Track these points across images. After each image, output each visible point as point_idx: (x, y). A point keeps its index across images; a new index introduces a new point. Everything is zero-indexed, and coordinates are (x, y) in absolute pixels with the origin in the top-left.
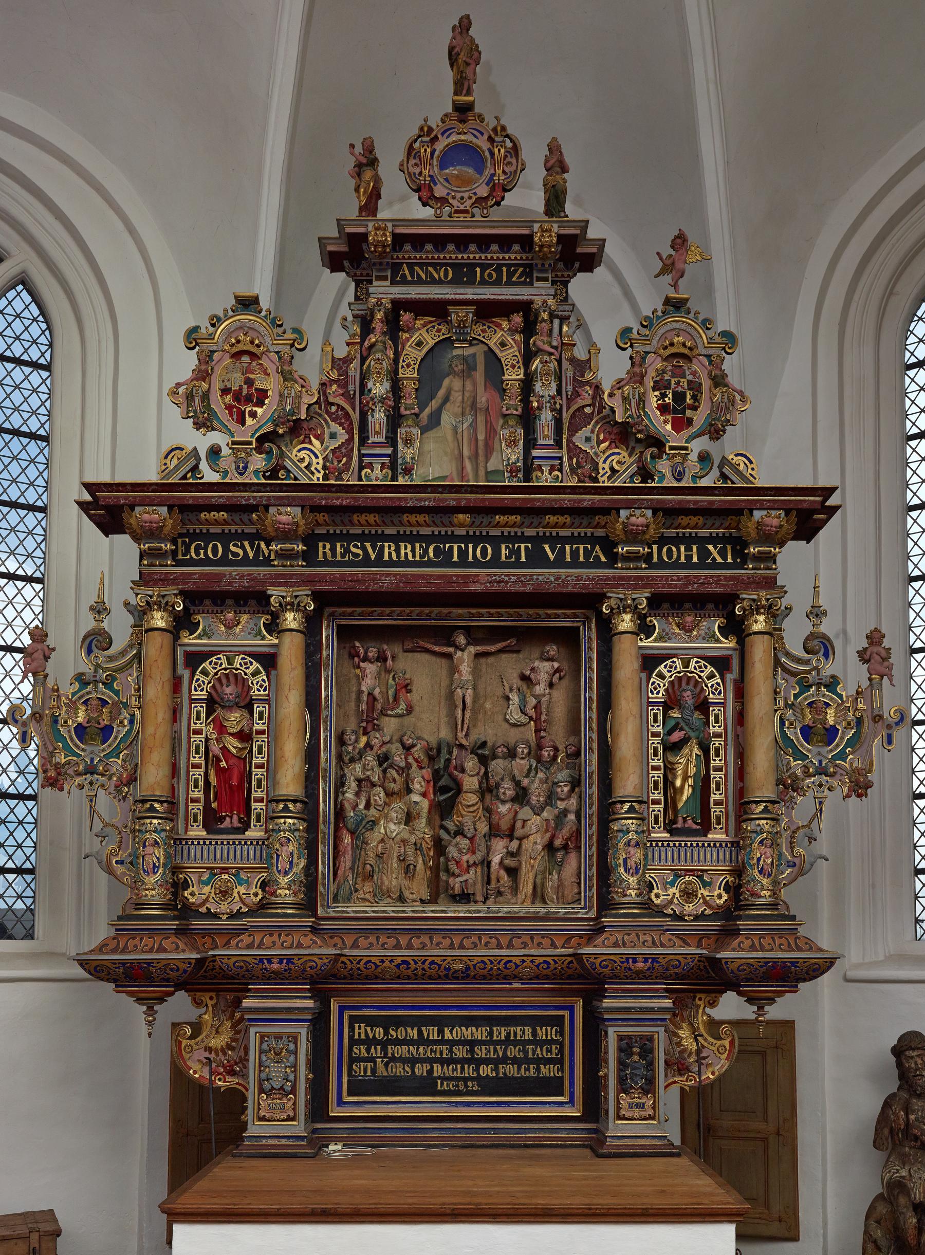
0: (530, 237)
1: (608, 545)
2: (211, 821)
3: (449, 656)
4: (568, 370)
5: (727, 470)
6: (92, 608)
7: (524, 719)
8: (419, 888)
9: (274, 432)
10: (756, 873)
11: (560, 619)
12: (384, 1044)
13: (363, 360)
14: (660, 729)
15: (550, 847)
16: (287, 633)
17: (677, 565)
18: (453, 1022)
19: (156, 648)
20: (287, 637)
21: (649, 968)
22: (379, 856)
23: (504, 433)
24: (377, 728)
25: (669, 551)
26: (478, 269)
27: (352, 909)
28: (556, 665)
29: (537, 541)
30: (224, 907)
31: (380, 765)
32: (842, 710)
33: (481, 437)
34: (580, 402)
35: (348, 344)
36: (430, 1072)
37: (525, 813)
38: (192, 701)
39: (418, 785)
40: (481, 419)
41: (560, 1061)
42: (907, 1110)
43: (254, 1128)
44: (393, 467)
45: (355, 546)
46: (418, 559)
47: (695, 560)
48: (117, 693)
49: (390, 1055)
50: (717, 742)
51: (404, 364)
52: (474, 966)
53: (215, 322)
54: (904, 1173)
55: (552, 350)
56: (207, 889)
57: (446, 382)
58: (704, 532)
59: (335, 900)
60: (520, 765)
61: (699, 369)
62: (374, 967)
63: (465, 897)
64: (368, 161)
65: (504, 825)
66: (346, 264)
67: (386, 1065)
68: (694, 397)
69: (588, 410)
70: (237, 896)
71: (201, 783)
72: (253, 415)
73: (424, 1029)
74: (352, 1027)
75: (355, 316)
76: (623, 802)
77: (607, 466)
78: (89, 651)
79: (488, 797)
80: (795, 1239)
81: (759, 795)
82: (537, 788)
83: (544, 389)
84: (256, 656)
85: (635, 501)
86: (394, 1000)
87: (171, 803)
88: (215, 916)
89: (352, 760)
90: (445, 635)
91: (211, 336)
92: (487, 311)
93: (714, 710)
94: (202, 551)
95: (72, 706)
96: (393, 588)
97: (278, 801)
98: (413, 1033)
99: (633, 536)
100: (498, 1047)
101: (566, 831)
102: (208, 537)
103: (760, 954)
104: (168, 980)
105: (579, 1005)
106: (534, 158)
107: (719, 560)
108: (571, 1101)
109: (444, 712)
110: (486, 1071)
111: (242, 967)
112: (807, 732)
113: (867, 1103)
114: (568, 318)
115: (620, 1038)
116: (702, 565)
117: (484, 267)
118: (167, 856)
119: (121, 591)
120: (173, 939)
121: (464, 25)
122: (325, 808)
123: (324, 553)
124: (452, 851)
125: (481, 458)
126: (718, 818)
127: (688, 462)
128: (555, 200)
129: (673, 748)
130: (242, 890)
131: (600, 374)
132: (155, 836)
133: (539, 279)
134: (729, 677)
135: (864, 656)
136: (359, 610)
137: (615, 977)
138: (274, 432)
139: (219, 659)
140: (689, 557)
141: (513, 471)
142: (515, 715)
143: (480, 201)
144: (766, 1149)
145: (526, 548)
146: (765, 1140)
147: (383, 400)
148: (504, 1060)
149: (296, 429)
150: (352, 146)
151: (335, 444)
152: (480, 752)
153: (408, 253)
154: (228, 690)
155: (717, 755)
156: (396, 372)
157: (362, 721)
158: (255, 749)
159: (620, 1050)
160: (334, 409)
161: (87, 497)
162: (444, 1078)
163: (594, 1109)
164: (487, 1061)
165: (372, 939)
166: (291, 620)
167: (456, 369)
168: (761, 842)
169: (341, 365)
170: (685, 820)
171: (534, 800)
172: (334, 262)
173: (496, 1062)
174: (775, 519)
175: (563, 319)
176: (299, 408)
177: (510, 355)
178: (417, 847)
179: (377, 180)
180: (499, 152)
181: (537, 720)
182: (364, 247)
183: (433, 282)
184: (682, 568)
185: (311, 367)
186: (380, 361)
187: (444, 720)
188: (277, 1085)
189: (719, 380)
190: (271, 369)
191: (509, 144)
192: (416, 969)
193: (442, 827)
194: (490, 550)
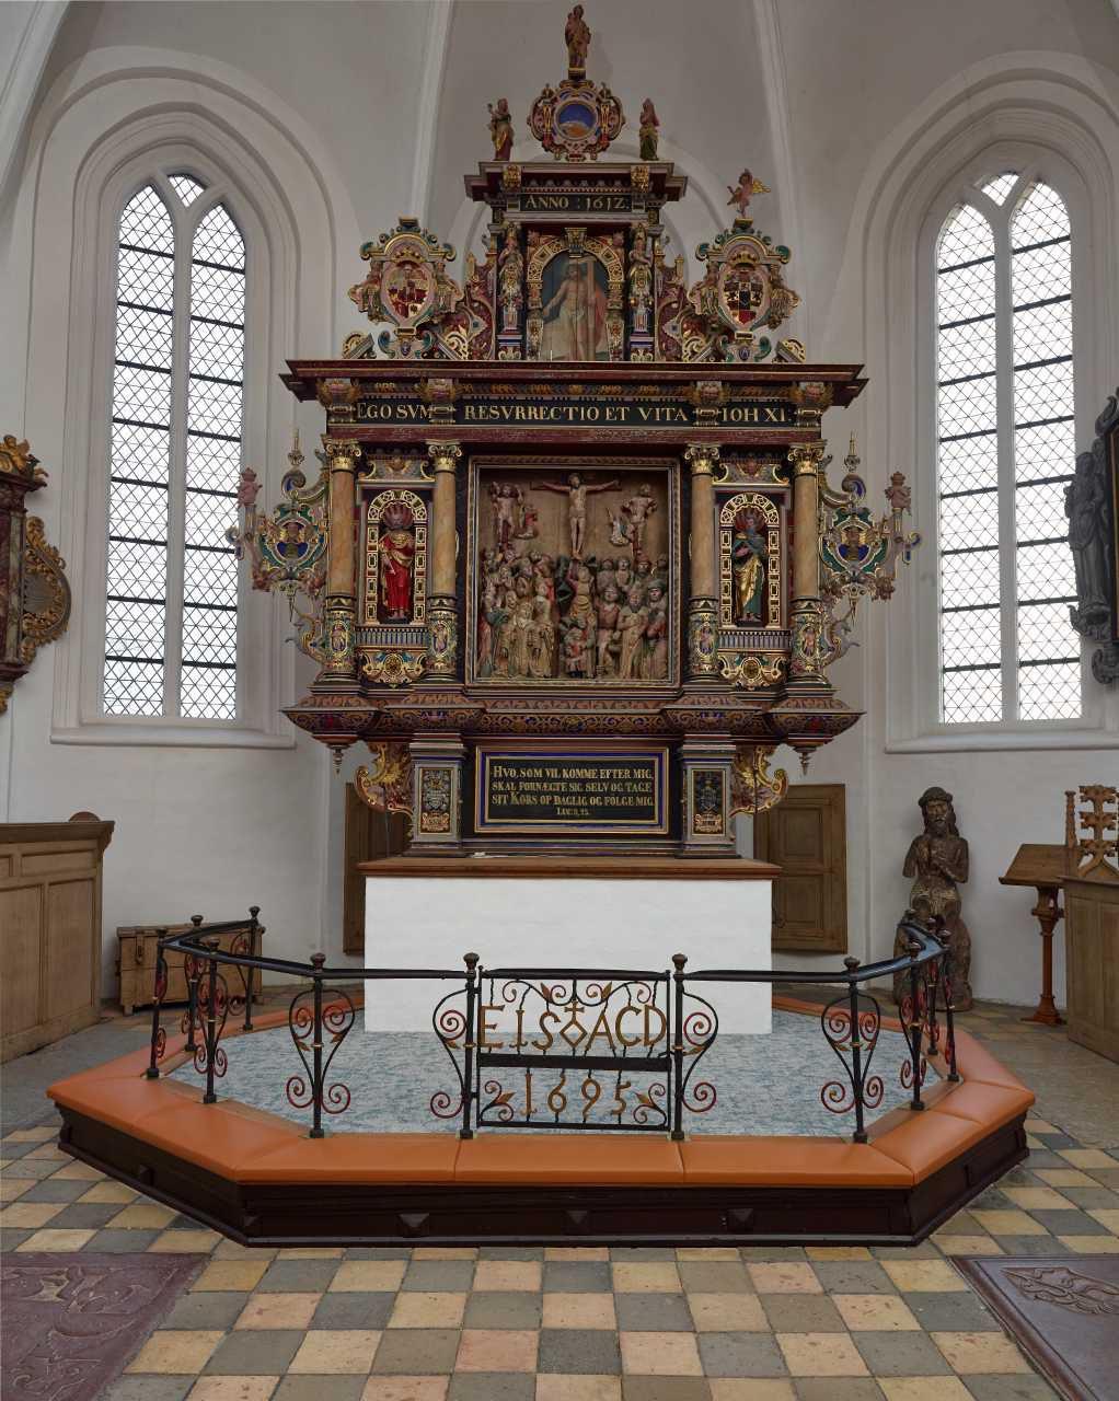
0: (629, 175)
1: (688, 408)
2: (383, 614)
3: (566, 493)
4: (659, 277)
5: (782, 352)
6: (290, 456)
7: (625, 541)
9: (431, 323)
10: (801, 652)
11: (653, 464)
12: (517, 781)
13: (499, 268)
15: (644, 637)
17: (742, 423)
18: (570, 765)
19: (339, 485)
20: (441, 477)
22: (513, 643)
23: (609, 323)
24: (510, 547)
25: (736, 413)
27: (492, 681)
28: (650, 500)
29: (634, 405)
30: (393, 679)
32: (871, 533)
33: (591, 326)
34: (668, 300)
35: (487, 256)
36: (552, 801)
37: (625, 610)
38: (368, 525)
39: (542, 589)
40: (591, 312)
41: (653, 795)
42: (930, 847)
43: (419, 837)
44: (523, 350)
47: (756, 419)
48: (310, 519)
50: (773, 557)
54: (926, 893)
56: (380, 665)
57: (564, 285)
58: (763, 399)
59: (479, 675)
60: (621, 575)
61: (761, 275)
63: (579, 674)
64: (502, 118)
65: (609, 619)
66: (486, 194)
67: (518, 796)
68: (757, 296)
69: (675, 306)
71: (376, 586)
72: (414, 309)
74: (492, 769)
75: (493, 235)
76: (699, 600)
77: (688, 349)
78: (288, 488)
79: (597, 599)
81: (803, 595)
82: (635, 593)
83: (640, 290)
84: (418, 492)
85: (709, 375)
86: (525, 748)
88: (387, 686)
89: (491, 571)
90: (563, 477)
91: (381, 250)
92: (595, 231)
93: (771, 534)
95: (275, 529)
96: (523, 440)
97: (434, 598)
98: (539, 773)
99: (708, 401)
101: (657, 625)
102: (380, 402)
103: (801, 710)
104: (352, 728)
105: (666, 753)
106: (632, 114)
108: (660, 823)
109: (562, 535)
110: (595, 801)
112: (844, 550)
113: (899, 846)
114: (658, 236)
115: (697, 774)
116: (761, 423)
117: (593, 198)
118: (352, 639)
119: (313, 442)
120: (356, 698)
121: (578, 12)
122: (471, 605)
124: (569, 639)
125: (591, 344)
126: (774, 614)
127: (757, 341)
128: (648, 148)
129: (739, 561)
130: (407, 665)
132: (341, 623)
133: (636, 207)
134: (783, 508)
135: (890, 494)
136: (496, 457)
137: (692, 728)
138: (431, 323)
140: (751, 418)
141: (616, 353)
142: (617, 537)
143: (590, 148)
148: (609, 793)
149: (449, 320)
150: (490, 106)
153: (534, 186)
154: (396, 517)
155: (774, 567)
156: (525, 277)
158: (417, 561)
159: (696, 782)
160: (476, 305)
161: (288, 372)
162: (562, 807)
163: (677, 828)
164: (595, 794)
165: (507, 703)
166: (444, 464)
168: (806, 630)
169: (481, 271)
170: (748, 616)
171: (632, 601)
172: (477, 193)
173: (602, 795)
174: (816, 388)
175: (655, 237)
177: (614, 263)
178: (542, 636)
179: (510, 132)
180: (605, 110)
181: (634, 542)
183: (554, 209)
184: (747, 426)
185: (457, 272)
186: (513, 269)
187: (562, 541)
188: (436, 806)
189: (776, 284)
190: (428, 275)
191: (613, 104)
193: (561, 621)
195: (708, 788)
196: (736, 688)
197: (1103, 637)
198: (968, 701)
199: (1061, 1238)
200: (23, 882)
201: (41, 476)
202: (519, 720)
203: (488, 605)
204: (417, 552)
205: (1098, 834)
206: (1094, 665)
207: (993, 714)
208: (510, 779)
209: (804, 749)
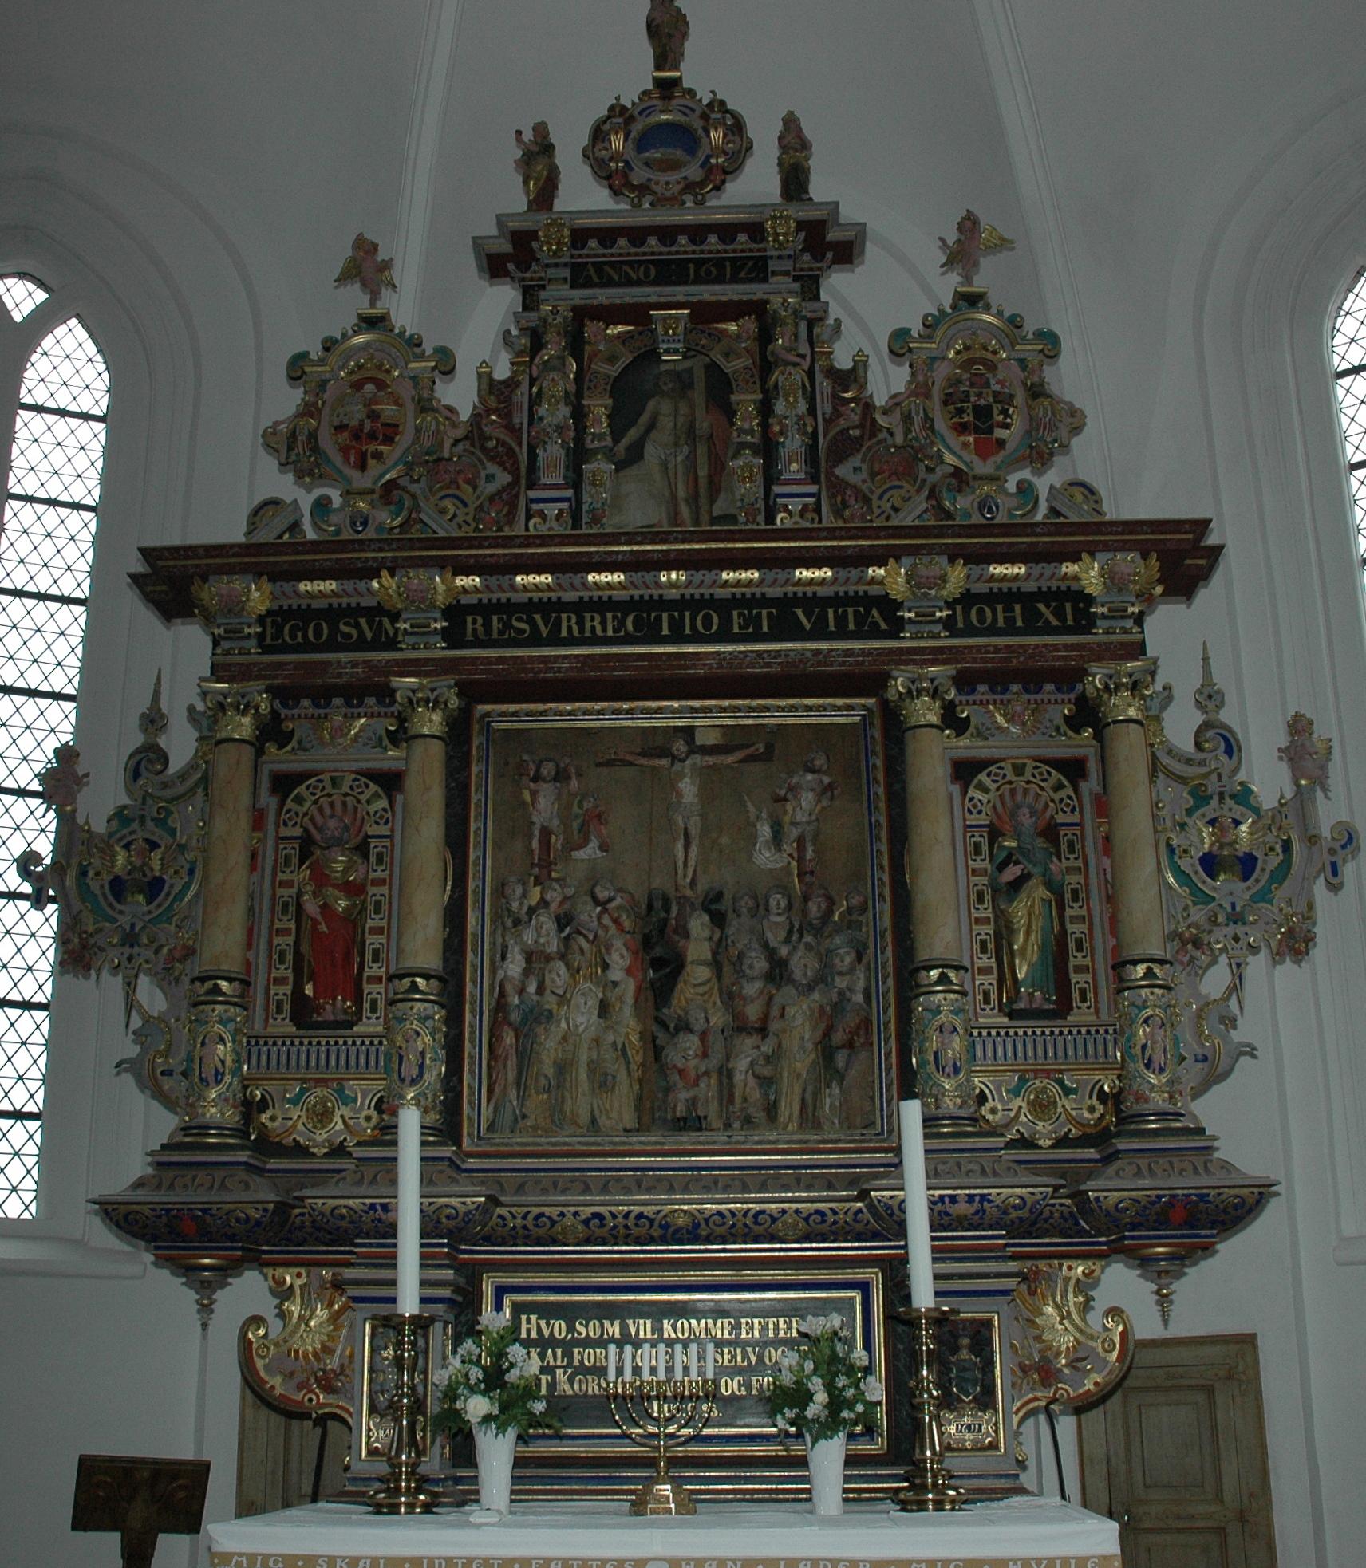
4: (824, 385)
8: (620, 1108)
12: (567, 1347)
14: (987, 865)
15: (827, 1052)
16: (420, 741)
21: (977, 1212)
25: (981, 612)
26: (691, 266)
28: (826, 780)
31: (561, 929)
33: (703, 472)
40: (701, 450)
45: (519, 620)
46: (610, 633)
47: (1019, 623)
49: (577, 1363)
51: (592, 385)
52: (707, 1220)
53: (329, 345)
55: (798, 360)
57: (651, 405)
62: (548, 1224)
65: (753, 1012)
66: (511, 267)
67: (571, 1381)
70: (340, 1122)
73: (630, 1322)
82: (802, 964)
87: (246, 983)
88: (300, 1151)
94: (300, 634)
97: (401, 977)
100: (749, 1349)
106: (764, 136)
107: (1055, 622)
111: (343, 1217)
116: (1029, 630)
123: (474, 630)
124: (673, 1056)
128: (795, 181)
130: (346, 1111)
131: (871, 388)
134: (1084, 786)
139: (320, 781)
140: (1009, 621)
144: (1224, 1545)
145: (769, 614)
146: (1221, 1531)
147: (560, 429)
150: (519, 133)
151: (491, 488)
152: (713, 907)
157: (533, 865)
158: (371, 908)
167: (665, 388)
172: (495, 267)
176: (441, 445)
182: (535, 245)
189: (1037, 392)
192: (615, 1227)
194: (716, 619)
195: (964, 1354)
196: (1010, 1145)
202: (569, 1221)
204: (372, 890)
208: (551, 1342)
209: (1162, 1273)
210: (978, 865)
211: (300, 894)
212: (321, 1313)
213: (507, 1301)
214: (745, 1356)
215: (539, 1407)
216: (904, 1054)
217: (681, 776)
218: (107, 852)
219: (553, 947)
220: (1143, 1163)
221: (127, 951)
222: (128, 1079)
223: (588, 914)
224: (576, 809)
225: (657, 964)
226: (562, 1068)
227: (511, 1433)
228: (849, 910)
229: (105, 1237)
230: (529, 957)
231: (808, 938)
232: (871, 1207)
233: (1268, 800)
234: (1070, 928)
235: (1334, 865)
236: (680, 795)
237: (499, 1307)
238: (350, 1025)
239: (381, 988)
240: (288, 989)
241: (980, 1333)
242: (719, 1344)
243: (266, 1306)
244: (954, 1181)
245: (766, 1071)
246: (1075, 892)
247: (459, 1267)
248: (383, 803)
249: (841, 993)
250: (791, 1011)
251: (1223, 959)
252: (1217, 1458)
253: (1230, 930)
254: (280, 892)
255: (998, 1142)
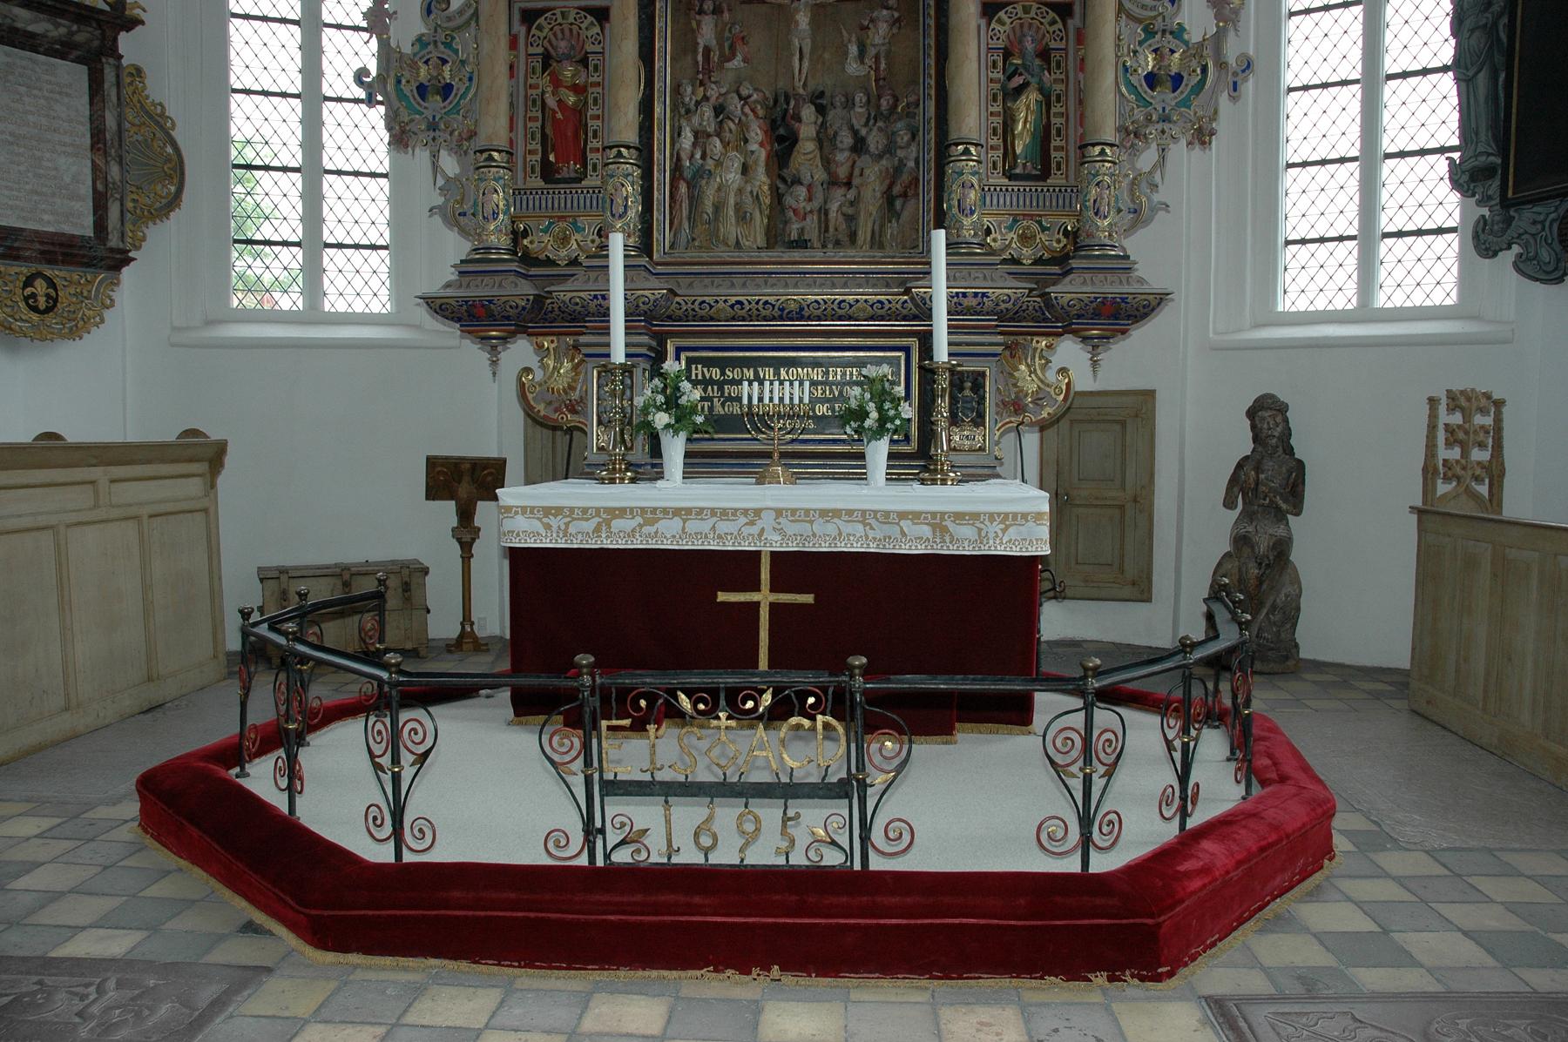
8: (756, 234)
12: (721, 385)
14: (1000, 75)
15: (889, 199)
27: (690, 255)
28: (896, 15)
31: (717, 116)
42: (1258, 469)
65: (842, 172)
67: (723, 405)
80: (1149, 600)
82: (875, 141)
88: (550, 262)
97: (611, 148)
101: (905, 178)
104: (508, 318)
124: (789, 200)
130: (578, 237)
134: (1070, 22)
144: (1123, 516)
146: (1122, 507)
158: (590, 101)
195: (967, 393)
196: (1004, 261)
197: (1490, 198)
198: (1314, 283)
199: (1373, 927)
200: (115, 513)
201: (137, 11)
202: (721, 305)
203: (684, 156)
204: (590, 90)
205: (1465, 454)
206: (1476, 236)
207: (1346, 300)
208: (711, 382)
209: (1095, 345)
210: (995, 75)
211: (543, 93)
212: (567, 365)
213: (683, 356)
214: (831, 391)
215: (699, 419)
216: (939, 200)
217: (797, 10)
218: (413, 66)
219: (711, 129)
220: (1088, 276)
221: (432, 134)
222: (437, 219)
223: (735, 105)
224: (727, 34)
225: (780, 139)
226: (718, 208)
227: (683, 436)
228: (908, 105)
229: (422, 314)
230: (696, 134)
231: (880, 124)
232: (912, 299)
233: (1195, 37)
234: (1053, 120)
235: (1235, 84)
236: (797, 23)
237: (678, 358)
238: (580, 180)
239: (599, 155)
240: (539, 157)
241: (978, 381)
242: (813, 383)
243: (533, 361)
244: (963, 284)
245: (850, 211)
246: (1058, 97)
247: (654, 335)
248: (597, 29)
249: (901, 160)
250: (867, 172)
251: (1154, 146)
252: (1123, 463)
253: (1160, 126)
254: (530, 92)
255: (997, 259)
